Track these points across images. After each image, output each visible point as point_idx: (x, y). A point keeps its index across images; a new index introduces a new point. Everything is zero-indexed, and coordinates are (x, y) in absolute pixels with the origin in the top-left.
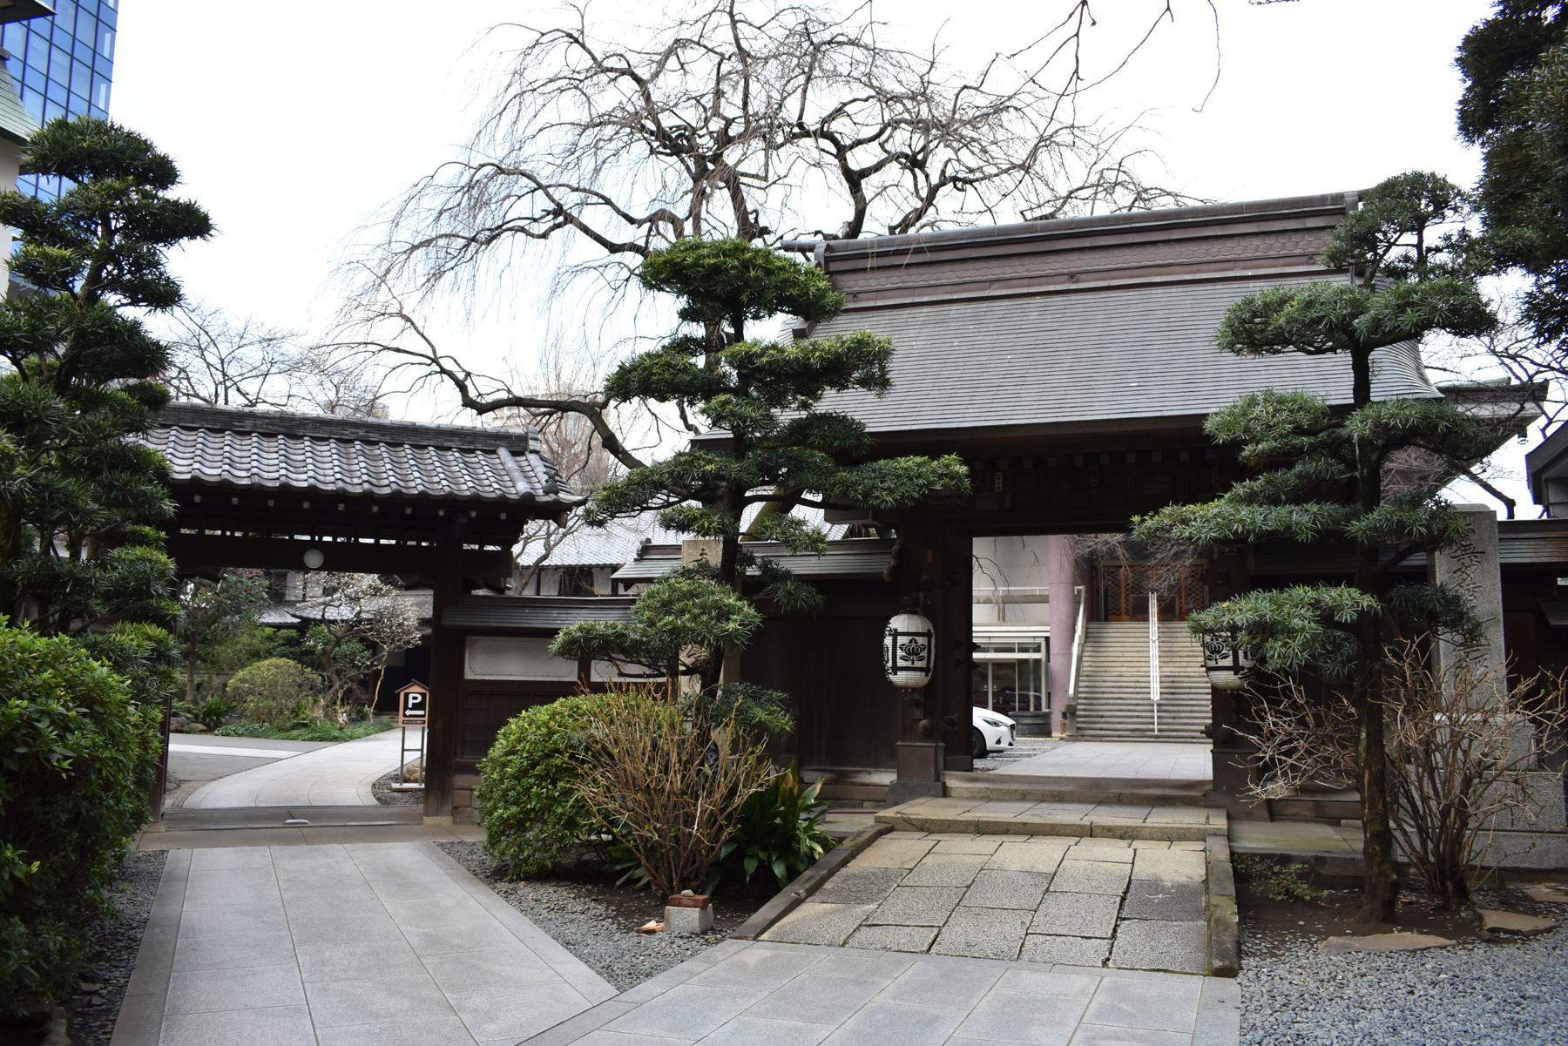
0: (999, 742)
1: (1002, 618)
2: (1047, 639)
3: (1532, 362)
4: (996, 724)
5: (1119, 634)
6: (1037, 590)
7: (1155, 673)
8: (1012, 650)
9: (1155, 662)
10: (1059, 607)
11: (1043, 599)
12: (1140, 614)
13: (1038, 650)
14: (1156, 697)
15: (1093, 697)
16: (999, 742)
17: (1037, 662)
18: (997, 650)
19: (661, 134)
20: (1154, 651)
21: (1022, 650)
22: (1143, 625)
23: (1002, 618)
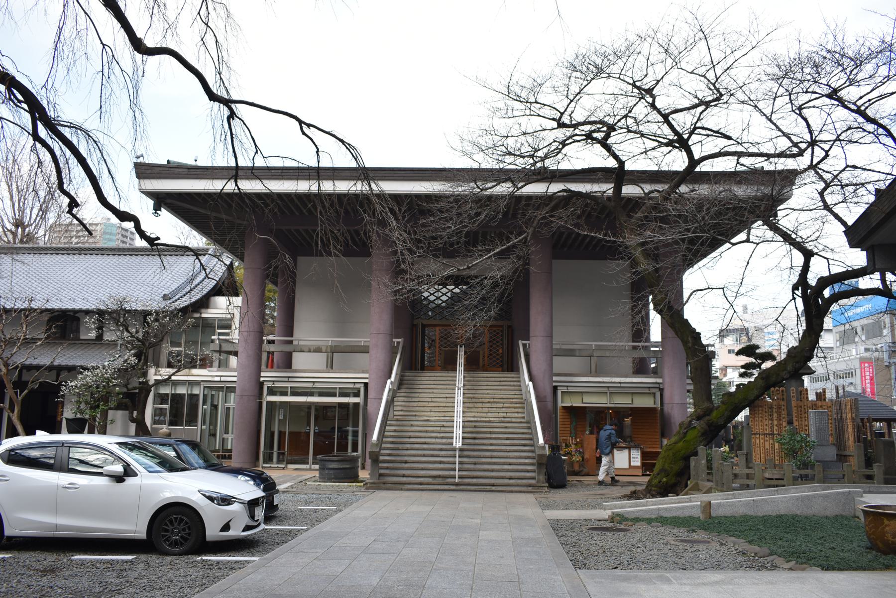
0: (226, 527)
1: (330, 366)
2: (366, 384)
3: (825, 142)
4: (226, 500)
5: (430, 383)
6: (362, 341)
7: (459, 419)
8: (333, 395)
9: (459, 408)
10: (377, 356)
11: (365, 350)
12: (450, 365)
13: (357, 395)
14: (458, 444)
15: (399, 443)
16: (226, 527)
17: (356, 405)
18: (321, 394)
19: (437, 249)
20: (459, 398)
21: (342, 394)
22: (631, 338)
23: (330, 366)
